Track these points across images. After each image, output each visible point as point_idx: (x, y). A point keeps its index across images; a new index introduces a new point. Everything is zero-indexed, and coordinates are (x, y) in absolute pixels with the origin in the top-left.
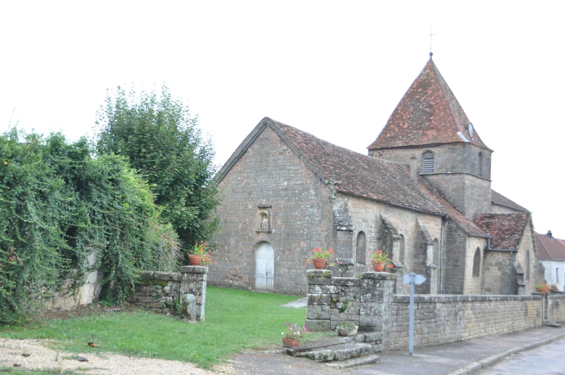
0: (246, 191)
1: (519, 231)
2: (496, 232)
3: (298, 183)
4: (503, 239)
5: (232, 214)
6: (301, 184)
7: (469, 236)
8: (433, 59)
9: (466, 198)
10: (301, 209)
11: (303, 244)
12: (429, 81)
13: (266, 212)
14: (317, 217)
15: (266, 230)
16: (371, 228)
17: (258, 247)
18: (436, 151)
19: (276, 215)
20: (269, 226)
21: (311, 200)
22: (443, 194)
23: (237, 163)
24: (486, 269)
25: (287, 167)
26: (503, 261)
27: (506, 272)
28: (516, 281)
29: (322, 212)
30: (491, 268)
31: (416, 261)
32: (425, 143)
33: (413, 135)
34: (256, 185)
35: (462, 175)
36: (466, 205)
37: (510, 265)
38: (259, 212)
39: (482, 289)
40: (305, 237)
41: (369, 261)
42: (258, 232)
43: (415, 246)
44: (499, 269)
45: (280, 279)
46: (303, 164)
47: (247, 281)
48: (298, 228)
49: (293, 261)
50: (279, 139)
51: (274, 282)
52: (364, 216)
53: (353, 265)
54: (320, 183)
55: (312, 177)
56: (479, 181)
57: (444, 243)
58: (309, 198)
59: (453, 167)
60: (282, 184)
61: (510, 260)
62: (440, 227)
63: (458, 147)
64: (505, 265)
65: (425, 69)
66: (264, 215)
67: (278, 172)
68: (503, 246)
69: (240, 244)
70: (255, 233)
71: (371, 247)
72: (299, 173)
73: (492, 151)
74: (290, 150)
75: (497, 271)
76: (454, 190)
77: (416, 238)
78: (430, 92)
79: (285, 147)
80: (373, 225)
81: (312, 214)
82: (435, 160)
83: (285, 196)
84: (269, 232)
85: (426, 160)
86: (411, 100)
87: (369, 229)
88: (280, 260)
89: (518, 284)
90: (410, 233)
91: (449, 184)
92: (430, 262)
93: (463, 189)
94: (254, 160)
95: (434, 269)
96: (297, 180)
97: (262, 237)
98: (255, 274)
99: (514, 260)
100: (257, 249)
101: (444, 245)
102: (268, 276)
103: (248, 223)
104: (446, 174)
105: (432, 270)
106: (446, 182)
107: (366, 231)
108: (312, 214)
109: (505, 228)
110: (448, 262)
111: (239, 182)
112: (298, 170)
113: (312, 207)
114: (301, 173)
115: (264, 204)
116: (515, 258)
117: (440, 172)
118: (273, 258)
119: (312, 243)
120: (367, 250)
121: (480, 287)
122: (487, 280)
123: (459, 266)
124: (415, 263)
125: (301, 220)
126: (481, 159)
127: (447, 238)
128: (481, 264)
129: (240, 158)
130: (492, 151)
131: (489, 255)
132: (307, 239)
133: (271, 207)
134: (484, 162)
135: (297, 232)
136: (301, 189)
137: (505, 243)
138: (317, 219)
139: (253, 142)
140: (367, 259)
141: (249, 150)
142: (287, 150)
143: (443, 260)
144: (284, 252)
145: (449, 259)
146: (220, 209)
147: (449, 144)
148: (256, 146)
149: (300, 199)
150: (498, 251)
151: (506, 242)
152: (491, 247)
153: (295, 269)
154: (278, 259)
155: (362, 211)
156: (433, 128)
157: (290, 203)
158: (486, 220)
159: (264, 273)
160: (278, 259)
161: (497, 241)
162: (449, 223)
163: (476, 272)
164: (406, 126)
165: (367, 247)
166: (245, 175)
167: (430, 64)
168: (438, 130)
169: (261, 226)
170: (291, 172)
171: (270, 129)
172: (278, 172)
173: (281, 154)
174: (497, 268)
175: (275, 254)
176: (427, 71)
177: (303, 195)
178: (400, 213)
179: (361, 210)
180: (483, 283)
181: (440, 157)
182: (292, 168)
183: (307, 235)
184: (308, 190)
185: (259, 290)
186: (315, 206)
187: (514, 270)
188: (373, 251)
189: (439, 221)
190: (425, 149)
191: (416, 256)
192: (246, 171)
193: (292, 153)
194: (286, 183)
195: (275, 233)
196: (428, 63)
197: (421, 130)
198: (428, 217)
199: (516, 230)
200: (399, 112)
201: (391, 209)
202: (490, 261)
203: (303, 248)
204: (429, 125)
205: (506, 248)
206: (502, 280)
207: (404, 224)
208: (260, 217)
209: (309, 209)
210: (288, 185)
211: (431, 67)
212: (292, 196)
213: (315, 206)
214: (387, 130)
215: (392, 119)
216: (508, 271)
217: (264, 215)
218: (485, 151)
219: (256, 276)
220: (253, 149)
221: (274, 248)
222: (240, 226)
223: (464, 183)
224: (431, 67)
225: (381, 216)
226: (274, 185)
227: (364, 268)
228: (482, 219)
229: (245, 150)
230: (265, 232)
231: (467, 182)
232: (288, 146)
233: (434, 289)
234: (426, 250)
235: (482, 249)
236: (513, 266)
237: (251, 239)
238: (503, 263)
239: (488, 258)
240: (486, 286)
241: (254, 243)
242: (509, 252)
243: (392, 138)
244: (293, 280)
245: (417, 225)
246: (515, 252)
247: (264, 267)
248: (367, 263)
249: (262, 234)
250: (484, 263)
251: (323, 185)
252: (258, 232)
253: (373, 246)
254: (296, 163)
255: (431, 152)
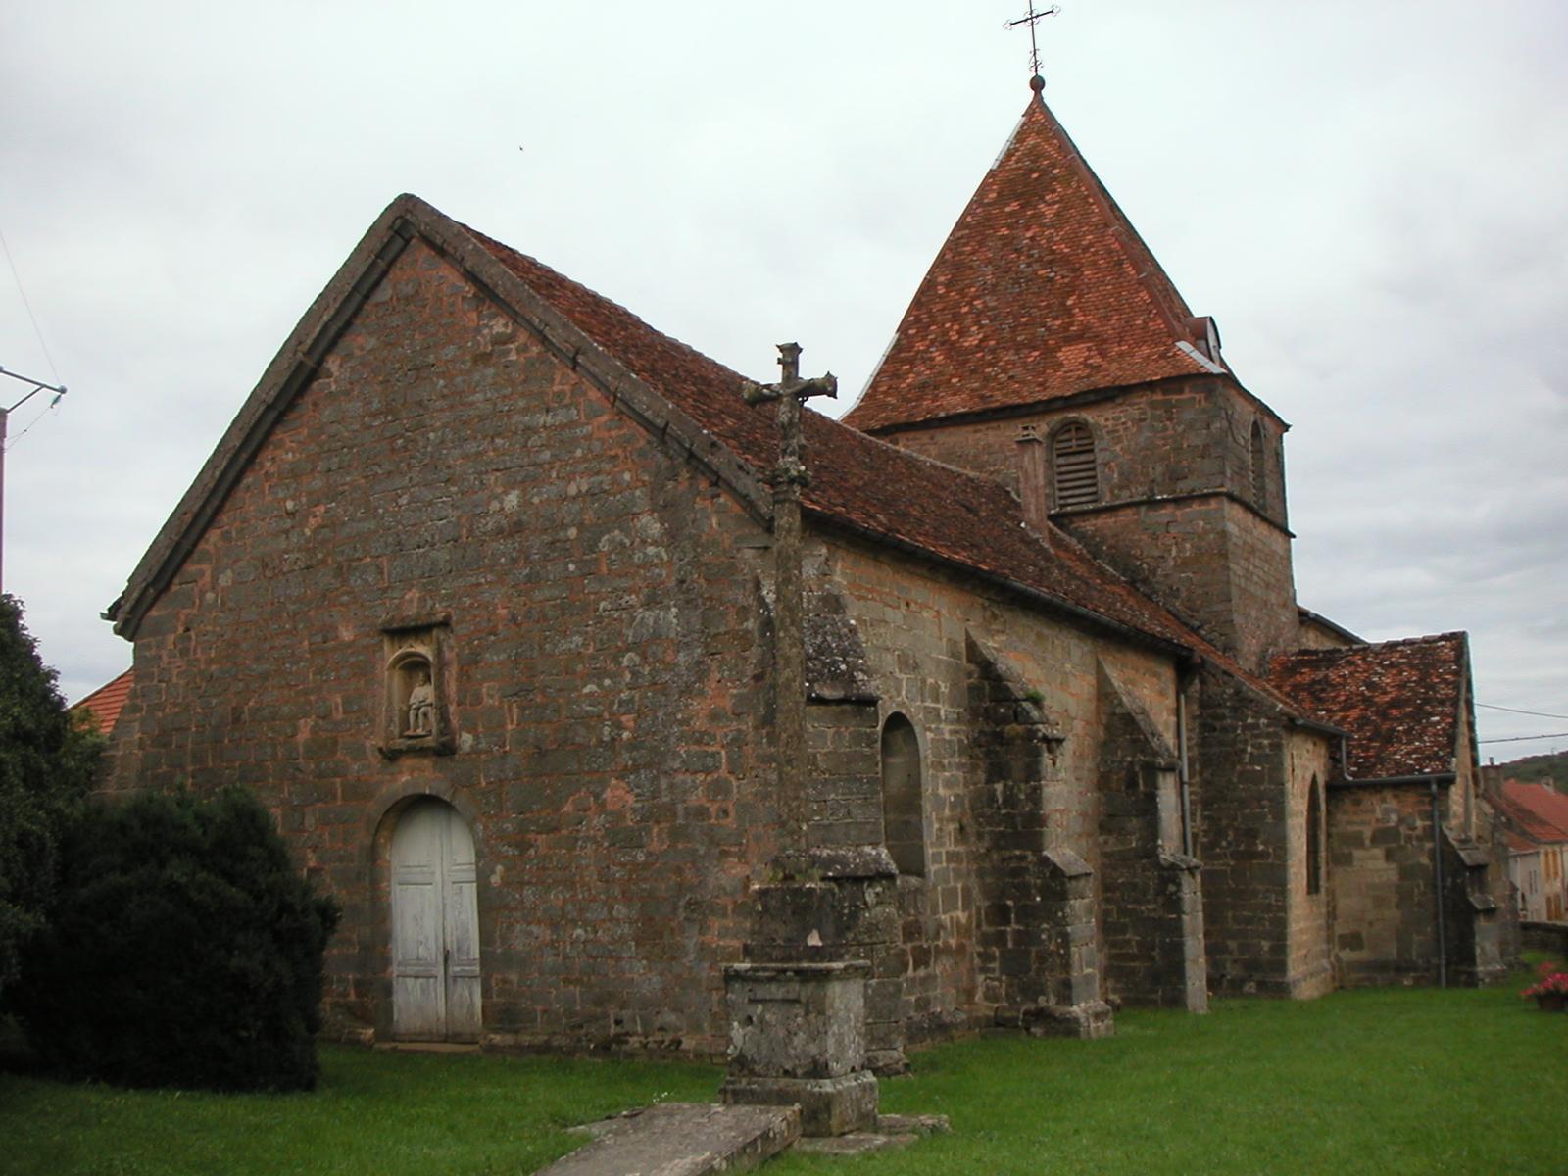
0: (323, 562)
1: (1442, 702)
2: (1354, 713)
3: (573, 490)
4: (1388, 739)
5: (265, 677)
6: (591, 494)
7: (1292, 726)
8: (1046, 101)
9: (1235, 592)
10: (599, 620)
11: (617, 793)
12: (1044, 172)
13: (423, 649)
14: (679, 647)
15: (430, 741)
16: (936, 700)
17: (394, 830)
18: (1102, 421)
19: (471, 663)
20: (444, 718)
21: (646, 564)
22: (1145, 581)
23: (280, 434)
24: (1341, 859)
25: (516, 418)
26: (1401, 821)
27: (1420, 865)
28: (1460, 892)
29: (706, 622)
30: (1358, 853)
31: (1113, 845)
32: (1059, 393)
33: (1004, 371)
34: (372, 525)
35: (1213, 504)
36: (1237, 619)
37: (1430, 833)
38: (391, 653)
39: (1329, 940)
40: (626, 758)
41: (936, 857)
42: (392, 756)
43: (1103, 782)
44: (1389, 856)
45: (514, 977)
46: (594, 394)
47: (352, 997)
48: (590, 715)
49: (570, 884)
50: (469, 289)
51: (486, 993)
52: (904, 641)
53: (890, 877)
54: (685, 475)
55: (642, 453)
56: (1262, 530)
57: (1190, 766)
58: (638, 557)
59: (1175, 476)
60: (495, 505)
61: (1430, 816)
62: (1171, 701)
63: (1186, 395)
64: (1409, 838)
65: (1021, 136)
66: (414, 667)
67: (472, 447)
68: (1397, 763)
69: (310, 821)
70: (375, 760)
71: (941, 791)
72: (575, 442)
73: (1286, 428)
74: (523, 337)
75: (1381, 864)
76: (1184, 564)
77: (1105, 747)
78: (1049, 212)
79: (499, 326)
80: (944, 688)
81: (656, 636)
82: (1100, 457)
83: (514, 561)
84: (446, 750)
85: (1062, 461)
86: (981, 244)
87: (929, 703)
88: (506, 883)
89: (1471, 906)
90: (1078, 725)
91: (1166, 539)
92: (1169, 848)
93: (1224, 555)
94: (355, 407)
95: (1191, 870)
96: (571, 478)
97: (411, 777)
98: (387, 961)
99: (1444, 815)
100: (390, 839)
101: (1190, 778)
102: (455, 969)
103: (339, 716)
104: (1151, 503)
105: (1185, 879)
106: (1155, 537)
107: (915, 712)
108: (656, 636)
109: (1387, 698)
110: (1214, 844)
111: (289, 523)
112: (572, 425)
113: (651, 602)
114: (588, 437)
115: (411, 611)
116: (1448, 809)
117: (1125, 497)
118: (473, 876)
119: (664, 783)
120: (927, 806)
121: (1323, 934)
122: (1344, 904)
123: (1264, 855)
124: (1106, 855)
125: (598, 675)
126: (1258, 451)
127: (1203, 743)
128: (1323, 838)
129: (292, 405)
130: (1286, 428)
131: (1347, 804)
132: (636, 769)
133: (445, 624)
134: (1269, 464)
135: (581, 736)
136: (589, 518)
137: (1400, 753)
138: (682, 657)
139: (348, 324)
140: (930, 851)
141: (333, 364)
142: (511, 339)
143: (1195, 836)
144: (523, 846)
145: (1216, 832)
146: (210, 661)
147: (1150, 386)
148: (362, 341)
149: (588, 571)
150: (1378, 787)
151: (1405, 749)
152: (1353, 774)
153: (585, 924)
154: (495, 879)
155: (895, 616)
156: (1079, 338)
157: (538, 595)
158: (1307, 676)
159: (431, 952)
160: (495, 879)
161: (1367, 749)
162: (1203, 682)
163: (1313, 886)
164: (971, 342)
165: (927, 790)
166: (318, 483)
167: (1039, 116)
168: (1101, 344)
169: (405, 724)
170: (534, 440)
171: (424, 253)
172: (472, 447)
173: (483, 358)
174: (1378, 852)
175: (479, 855)
176: (1031, 142)
177: (604, 544)
178: (1039, 636)
179: (890, 614)
180: (1332, 915)
181: (1119, 440)
182: (543, 419)
183: (634, 745)
184: (624, 517)
185: (416, 1037)
186: (667, 593)
187: (1446, 855)
188: (953, 806)
189: (1168, 674)
190: (1057, 418)
191: (1107, 823)
192: (322, 466)
193: (535, 350)
194: (512, 499)
195: (475, 750)
196: (1030, 113)
197: (1035, 349)
198: (1133, 658)
199: (1426, 701)
200: (941, 291)
201: (1008, 616)
202: (1351, 829)
203: (620, 816)
204: (1066, 327)
205: (1411, 770)
206: (1404, 897)
207: (1058, 678)
208: (397, 679)
209: (640, 613)
210: (525, 503)
211: (1039, 125)
212: (546, 558)
213: (667, 593)
214: (904, 361)
215: (918, 320)
216: (1425, 860)
217: (414, 667)
218: (1267, 420)
219: (395, 970)
220: (349, 356)
221: (471, 826)
222: (303, 736)
223: (1224, 535)
224: (1039, 125)
225: (971, 646)
226: (453, 515)
227: (918, 891)
228: (1291, 669)
229: (310, 363)
230: (422, 752)
231: (1231, 528)
232: (515, 317)
233: (1195, 962)
234: (1151, 798)
235: (1321, 780)
236: (1444, 838)
237: (358, 792)
238: (1403, 830)
239: (1341, 818)
240: (1340, 929)
241: (374, 809)
242: (1426, 784)
243: (924, 386)
244: (578, 982)
245: (1104, 693)
246: (1446, 783)
247: (430, 926)
248: (932, 868)
249: (407, 763)
250: (1329, 836)
251: (703, 485)
252: (392, 756)
253: (948, 784)
254: (560, 395)
255: (1081, 427)
